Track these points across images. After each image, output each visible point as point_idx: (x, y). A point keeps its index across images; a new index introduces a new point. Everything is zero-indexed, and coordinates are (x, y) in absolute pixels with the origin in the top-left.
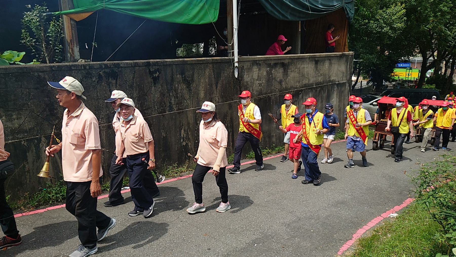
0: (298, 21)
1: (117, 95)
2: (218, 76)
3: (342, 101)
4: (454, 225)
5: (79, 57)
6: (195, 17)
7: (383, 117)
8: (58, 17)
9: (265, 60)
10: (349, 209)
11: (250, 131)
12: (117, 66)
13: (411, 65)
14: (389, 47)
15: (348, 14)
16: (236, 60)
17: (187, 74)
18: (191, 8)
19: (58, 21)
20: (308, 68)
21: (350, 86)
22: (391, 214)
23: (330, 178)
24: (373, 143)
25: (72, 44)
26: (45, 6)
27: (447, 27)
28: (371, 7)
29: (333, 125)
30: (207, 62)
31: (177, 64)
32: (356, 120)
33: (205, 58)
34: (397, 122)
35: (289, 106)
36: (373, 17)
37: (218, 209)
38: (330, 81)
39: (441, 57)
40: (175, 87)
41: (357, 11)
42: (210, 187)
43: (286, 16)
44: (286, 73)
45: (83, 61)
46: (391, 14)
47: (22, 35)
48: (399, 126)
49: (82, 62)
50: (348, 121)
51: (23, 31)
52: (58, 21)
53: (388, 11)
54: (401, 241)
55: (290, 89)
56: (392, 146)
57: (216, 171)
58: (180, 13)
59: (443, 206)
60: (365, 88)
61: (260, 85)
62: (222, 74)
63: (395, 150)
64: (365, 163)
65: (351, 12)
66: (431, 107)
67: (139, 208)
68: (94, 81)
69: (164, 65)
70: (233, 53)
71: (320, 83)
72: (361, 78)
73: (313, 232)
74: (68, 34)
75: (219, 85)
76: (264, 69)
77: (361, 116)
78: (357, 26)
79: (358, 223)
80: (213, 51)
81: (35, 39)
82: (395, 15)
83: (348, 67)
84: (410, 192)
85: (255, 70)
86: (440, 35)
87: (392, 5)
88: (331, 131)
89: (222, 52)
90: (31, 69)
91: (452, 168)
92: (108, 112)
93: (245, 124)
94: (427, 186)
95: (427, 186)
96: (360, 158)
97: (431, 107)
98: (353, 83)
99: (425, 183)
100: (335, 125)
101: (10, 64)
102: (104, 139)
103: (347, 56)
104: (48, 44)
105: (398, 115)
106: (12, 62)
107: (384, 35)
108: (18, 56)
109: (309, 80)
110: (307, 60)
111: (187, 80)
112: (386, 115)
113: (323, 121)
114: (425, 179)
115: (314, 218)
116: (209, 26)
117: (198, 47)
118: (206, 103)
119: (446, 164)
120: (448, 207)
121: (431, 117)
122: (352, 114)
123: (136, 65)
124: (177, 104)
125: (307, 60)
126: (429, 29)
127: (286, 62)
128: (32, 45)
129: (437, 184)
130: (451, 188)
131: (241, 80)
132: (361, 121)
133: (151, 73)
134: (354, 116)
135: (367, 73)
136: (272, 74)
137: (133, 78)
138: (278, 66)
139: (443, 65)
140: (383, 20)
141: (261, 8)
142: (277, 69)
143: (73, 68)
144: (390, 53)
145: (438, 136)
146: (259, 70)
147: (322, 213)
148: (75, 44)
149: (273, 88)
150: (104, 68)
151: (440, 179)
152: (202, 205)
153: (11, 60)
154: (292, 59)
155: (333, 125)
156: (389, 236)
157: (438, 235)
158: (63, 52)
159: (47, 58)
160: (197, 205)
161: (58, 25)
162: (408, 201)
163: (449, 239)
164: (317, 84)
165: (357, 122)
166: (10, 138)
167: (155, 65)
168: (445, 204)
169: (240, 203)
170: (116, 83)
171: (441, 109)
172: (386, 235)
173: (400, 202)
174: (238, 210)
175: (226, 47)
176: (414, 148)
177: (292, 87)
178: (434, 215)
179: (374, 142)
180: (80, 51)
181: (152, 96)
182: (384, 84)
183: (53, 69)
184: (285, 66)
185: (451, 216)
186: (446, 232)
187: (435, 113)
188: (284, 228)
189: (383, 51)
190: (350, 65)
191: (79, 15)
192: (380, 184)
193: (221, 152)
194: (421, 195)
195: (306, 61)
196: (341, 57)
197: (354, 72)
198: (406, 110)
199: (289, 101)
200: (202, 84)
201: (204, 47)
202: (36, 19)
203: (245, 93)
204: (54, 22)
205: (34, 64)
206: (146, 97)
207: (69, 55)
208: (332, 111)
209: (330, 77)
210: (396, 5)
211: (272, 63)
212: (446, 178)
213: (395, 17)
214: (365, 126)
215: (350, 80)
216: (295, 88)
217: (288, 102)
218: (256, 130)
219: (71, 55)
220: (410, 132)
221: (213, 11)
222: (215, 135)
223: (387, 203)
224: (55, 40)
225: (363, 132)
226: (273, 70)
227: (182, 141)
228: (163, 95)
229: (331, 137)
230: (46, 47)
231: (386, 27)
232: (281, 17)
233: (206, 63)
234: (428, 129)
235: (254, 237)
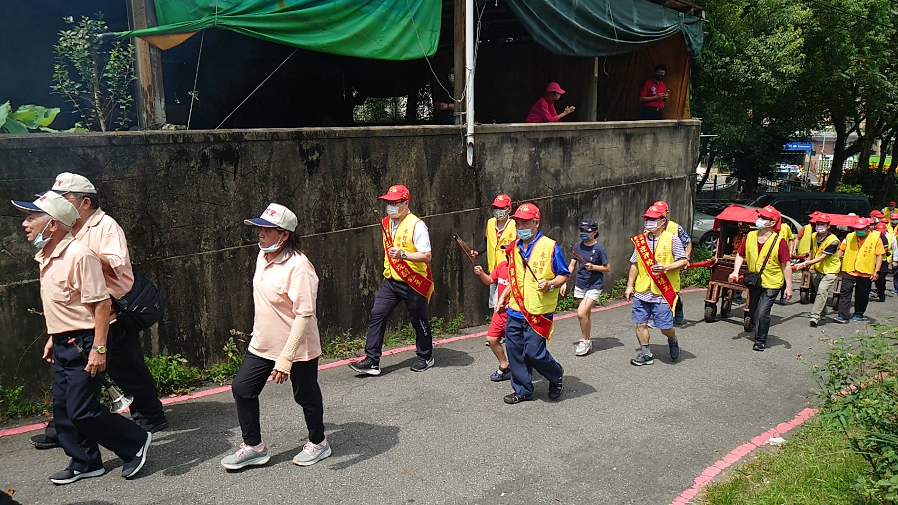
0: (593, 58)
1: (68, 185)
2: (434, 162)
3: (678, 213)
4: (894, 461)
5: (165, 120)
6: (392, 45)
7: (728, 249)
8: (126, 42)
9: (527, 132)
10: (688, 428)
11: (405, 279)
12: (238, 138)
13: (813, 146)
14: (770, 111)
15: (691, 44)
16: (471, 130)
17: (373, 156)
18: (385, 28)
19: (126, 50)
20: (612, 149)
21: (692, 186)
22: (772, 439)
23: (587, 390)
24: (706, 306)
25: (150, 95)
26: (101, 21)
27: (885, 74)
28: (736, 33)
29: (595, 267)
30: (414, 135)
31: (355, 137)
32: (652, 256)
33: (411, 126)
34: (756, 262)
35: (504, 221)
36: (740, 51)
37: (296, 459)
38: (653, 175)
39: (873, 132)
40: (350, 181)
41: (708, 39)
42: (280, 410)
43: (569, 46)
44: (567, 158)
45: (173, 127)
46: (776, 46)
47: (55, 76)
48: (761, 272)
49: (170, 129)
50: (635, 257)
51: (57, 67)
52: (126, 50)
53: (769, 41)
54: (789, 493)
55: (574, 189)
56: (746, 314)
57: (282, 373)
58: (362, 37)
59: (874, 423)
60: (723, 191)
61: (517, 180)
62: (442, 157)
63: (752, 322)
64: (674, 351)
65: (697, 41)
66: (833, 230)
67: (77, 464)
68: (193, 167)
69: (328, 138)
70: (465, 117)
71: (635, 179)
72: (714, 171)
73: (617, 471)
74: (144, 75)
75: (436, 180)
76: (526, 150)
77: (664, 248)
78: (707, 69)
79: (705, 454)
80: (425, 112)
81: (81, 83)
82: (783, 48)
83: (690, 148)
84: (808, 395)
85: (507, 150)
86: (871, 89)
87: (778, 29)
88: (591, 280)
89: (444, 116)
90: (70, 140)
91: (891, 351)
92: (218, 227)
93: (393, 260)
94: (842, 384)
95: (842, 384)
96: (663, 341)
97: (833, 230)
98: (700, 179)
99: (839, 378)
100: (601, 267)
101: (31, 131)
102: (209, 280)
103: (688, 127)
104: (104, 93)
105: (760, 246)
106: (34, 127)
107: (761, 88)
108: (46, 115)
109: (613, 173)
110: (610, 133)
111: (374, 168)
112: (736, 247)
113: (554, 256)
114: (839, 369)
115: (620, 443)
116: (419, 63)
117: (396, 102)
118: (273, 206)
119: (880, 341)
120: (883, 426)
121: (833, 249)
122: (643, 242)
123: (275, 137)
124: (353, 215)
125: (610, 133)
126: (851, 77)
127: (568, 136)
128: (73, 96)
129: (861, 382)
130: (889, 389)
131: (480, 170)
132: (664, 260)
133: (304, 153)
134: (647, 247)
135: (727, 160)
136: (540, 159)
137: (269, 162)
138: (553, 144)
139: (877, 146)
140: (760, 58)
141: (520, 29)
142: (551, 149)
143: (152, 141)
144: (772, 123)
145: (846, 292)
146: (515, 151)
147: (635, 434)
148: (157, 94)
149: (541, 186)
150: (213, 143)
151: (868, 372)
152: (259, 448)
153: (32, 123)
154: (580, 131)
155: (595, 267)
156: (767, 481)
157: (862, 480)
158: (134, 110)
159: (102, 121)
160: (247, 449)
161: (126, 56)
162: (806, 414)
163: (884, 489)
164: (627, 180)
165: (654, 262)
166: (27, 274)
167: (312, 139)
168: (877, 419)
169: (365, 441)
170: (236, 171)
171: (854, 233)
172: (760, 480)
173: (790, 415)
174: (353, 462)
175: (452, 105)
176: (797, 316)
177: (578, 186)
178: (855, 442)
179: (708, 305)
180: (167, 109)
181: (305, 197)
182: (759, 182)
183: (114, 142)
184: (565, 144)
185: (888, 444)
186: (878, 476)
187: (841, 241)
188: (560, 462)
189: (758, 118)
190: (693, 145)
191: (172, 37)
192: (750, 380)
193: (298, 324)
194: (829, 402)
195: (608, 136)
196: (676, 128)
197: (701, 159)
198: (777, 237)
199: (504, 211)
200: (401, 176)
201: (408, 105)
202: (83, 45)
203: (395, 191)
204: (119, 51)
205: (75, 131)
206: (294, 200)
207: (145, 115)
208: (596, 237)
209: (653, 168)
210: (786, 30)
211: (541, 137)
212: (880, 369)
213: (784, 52)
214: (673, 271)
215: (693, 174)
216: (584, 188)
217: (501, 213)
218: (418, 276)
219: (149, 116)
220: (784, 286)
221: (427, 34)
222: (285, 286)
223: (762, 416)
224: (119, 87)
225: (668, 283)
226: (543, 152)
227: (361, 286)
228: (325, 196)
229: (592, 294)
230: (101, 101)
231: (764, 72)
232: (559, 48)
233: (412, 136)
234: (829, 277)
235: (500, 479)
